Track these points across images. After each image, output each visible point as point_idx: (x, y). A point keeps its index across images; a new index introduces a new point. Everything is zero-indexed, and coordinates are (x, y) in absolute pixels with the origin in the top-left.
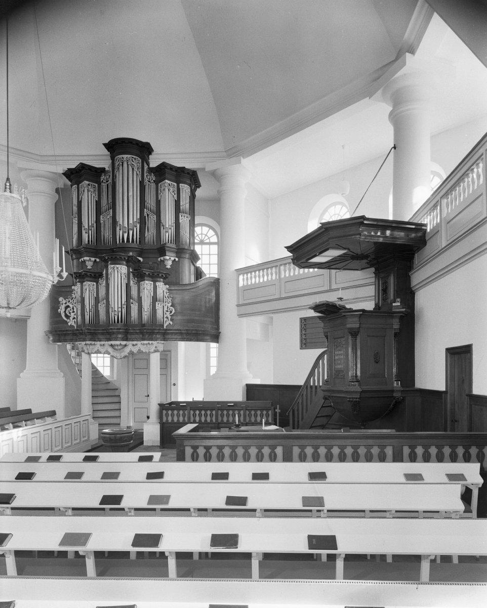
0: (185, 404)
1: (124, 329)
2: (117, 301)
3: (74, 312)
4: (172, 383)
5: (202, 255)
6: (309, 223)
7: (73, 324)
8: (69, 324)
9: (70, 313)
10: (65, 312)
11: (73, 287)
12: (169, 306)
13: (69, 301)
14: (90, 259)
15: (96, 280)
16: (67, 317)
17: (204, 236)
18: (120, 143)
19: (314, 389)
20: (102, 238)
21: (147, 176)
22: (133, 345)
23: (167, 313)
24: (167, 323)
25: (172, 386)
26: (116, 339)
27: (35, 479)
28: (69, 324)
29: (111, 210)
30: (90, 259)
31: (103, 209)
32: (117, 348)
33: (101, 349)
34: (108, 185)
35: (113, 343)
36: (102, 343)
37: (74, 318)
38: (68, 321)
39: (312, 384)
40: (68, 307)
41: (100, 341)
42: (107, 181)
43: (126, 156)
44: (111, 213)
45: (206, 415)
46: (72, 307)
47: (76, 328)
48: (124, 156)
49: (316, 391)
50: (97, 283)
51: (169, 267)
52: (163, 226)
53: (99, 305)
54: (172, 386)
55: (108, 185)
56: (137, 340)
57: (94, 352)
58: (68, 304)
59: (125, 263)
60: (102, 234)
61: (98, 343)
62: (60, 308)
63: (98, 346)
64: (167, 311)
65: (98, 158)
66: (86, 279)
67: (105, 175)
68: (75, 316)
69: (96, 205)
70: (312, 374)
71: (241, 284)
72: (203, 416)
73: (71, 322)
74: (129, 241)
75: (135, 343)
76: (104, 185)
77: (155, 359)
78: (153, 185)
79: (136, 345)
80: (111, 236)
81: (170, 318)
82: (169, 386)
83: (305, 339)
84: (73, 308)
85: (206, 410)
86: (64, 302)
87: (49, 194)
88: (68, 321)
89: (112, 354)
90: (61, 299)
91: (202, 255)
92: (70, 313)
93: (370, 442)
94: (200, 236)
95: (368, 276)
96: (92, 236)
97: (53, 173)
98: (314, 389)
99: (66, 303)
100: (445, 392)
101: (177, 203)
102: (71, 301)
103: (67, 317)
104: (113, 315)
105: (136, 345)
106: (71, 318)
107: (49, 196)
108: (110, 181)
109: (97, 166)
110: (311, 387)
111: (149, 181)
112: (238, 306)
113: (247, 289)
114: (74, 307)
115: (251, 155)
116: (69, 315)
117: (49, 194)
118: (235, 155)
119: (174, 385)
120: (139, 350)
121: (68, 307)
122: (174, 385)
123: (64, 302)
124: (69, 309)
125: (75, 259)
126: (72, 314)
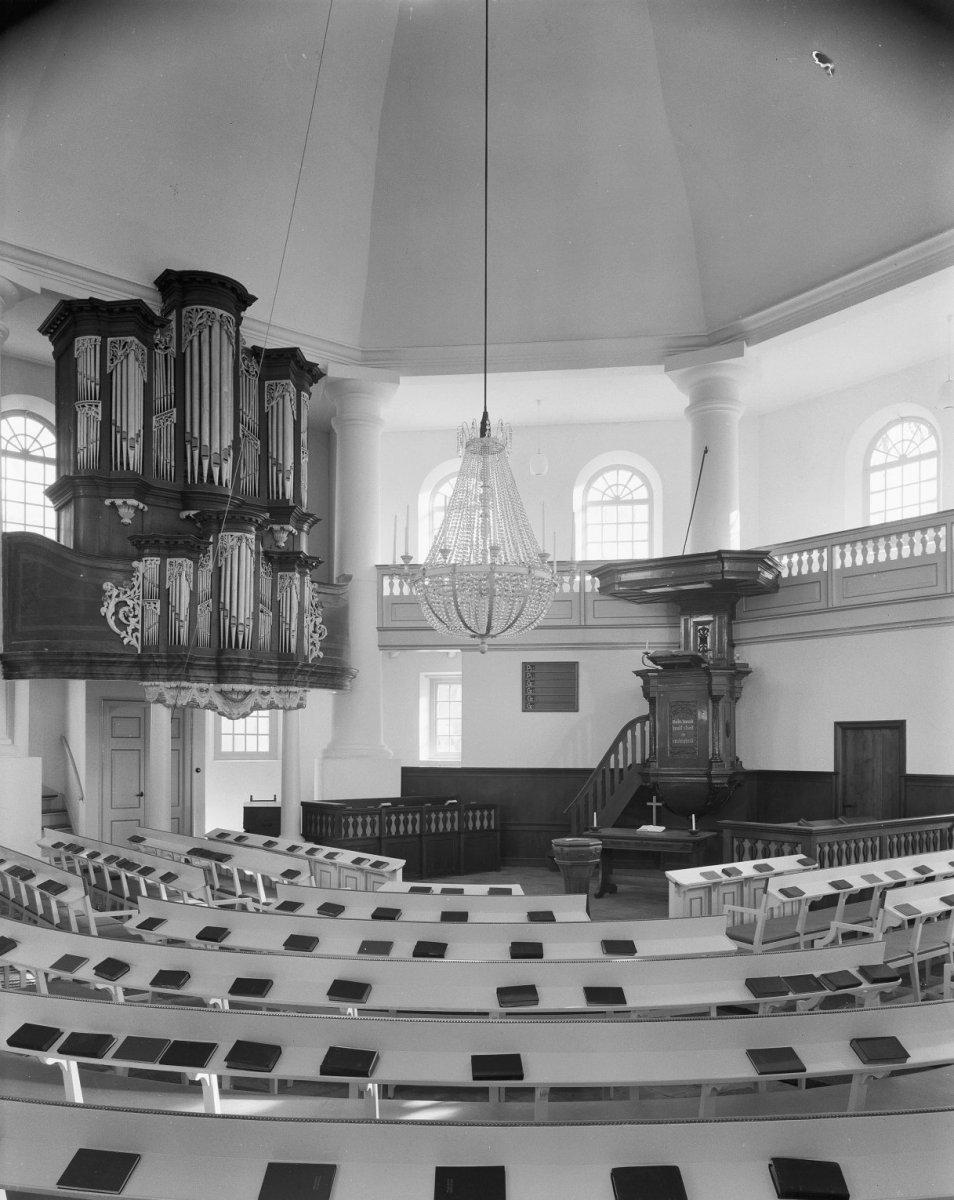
3: (135, 616)
4: (194, 769)
5: (45, 485)
6: (420, 496)
8: (125, 641)
9: (127, 618)
10: (116, 613)
11: (135, 564)
12: (317, 624)
13: (126, 592)
14: (125, 503)
15: (195, 556)
16: (122, 626)
18: (200, 282)
19: (617, 775)
20: (154, 464)
22: (201, 690)
24: (315, 654)
25: (195, 774)
27: (318, 951)
28: (125, 641)
29: (175, 410)
30: (125, 503)
32: (234, 696)
33: (265, 702)
34: (166, 356)
35: (226, 687)
36: (204, 686)
37: (135, 630)
38: (123, 634)
39: (612, 766)
40: (125, 604)
42: (166, 348)
43: (221, 312)
44: (175, 416)
45: (406, 823)
46: (131, 606)
48: (216, 310)
49: (621, 778)
50: (196, 562)
52: (277, 464)
54: (195, 774)
55: (166, 356)
58: (123, 598)
59: (253, 529)
60: (154, 455)
61: (196, 685)
62: (106, 604)
63: (195, 692)
64: (315, 632)
65: (22, 255)
67: (162, 334)
68: (139, 627)
69: (111, 383)
70: (613, 749)
71: (386, 592)
72: (360, 826)
73: (129, 639)
74: (213, 482)
75: (265, 688)
76: (159, 353)
78: (255, 381)
79: (188, 688)
81: (318, 645)
84: (134, 608)
88: (123, 634)
90: (107, 586)
91: (45, 485)
97: (14, 284)
98: (617, 775)
99: (118, 596)
100: (835, 773)
101: (148, 389)
102: (128, 593)
103: (122, 626)
105: (207, 690)
106: (129, 630)
108: (173, 349)
111: (247, 371)
112: (379, 629)
113: (397, 602)
114: (136, 607)
115: (416, 374)
116: (125, 621)
118: (18, 262)
119: (198, 771)
120: (193, 700)
121: (125, 604)
124: (126, 609)
126: (133, 621)
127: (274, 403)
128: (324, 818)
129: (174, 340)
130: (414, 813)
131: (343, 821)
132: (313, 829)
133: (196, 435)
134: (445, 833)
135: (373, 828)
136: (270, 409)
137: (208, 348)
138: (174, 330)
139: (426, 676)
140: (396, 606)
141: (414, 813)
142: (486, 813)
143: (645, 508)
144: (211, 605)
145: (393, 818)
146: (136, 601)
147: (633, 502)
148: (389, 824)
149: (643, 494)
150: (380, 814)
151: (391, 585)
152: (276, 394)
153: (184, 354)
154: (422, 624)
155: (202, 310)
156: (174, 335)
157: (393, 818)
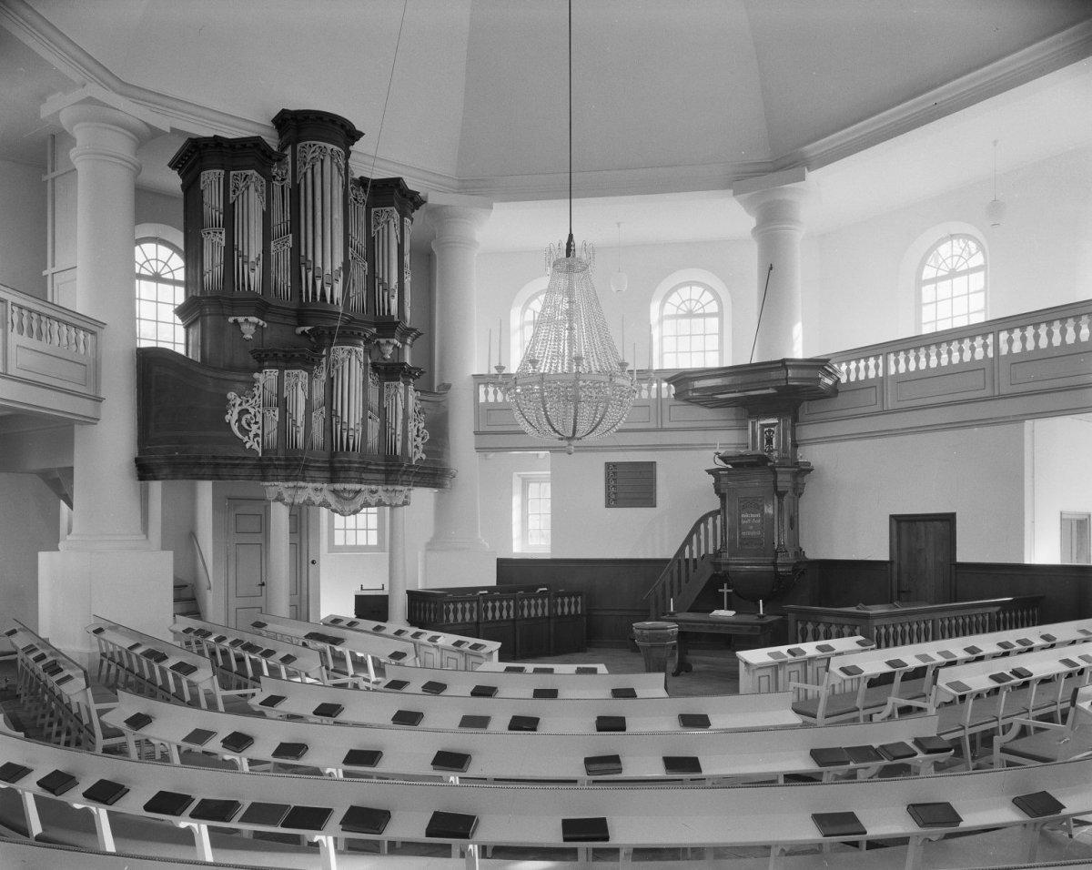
0: (486, 592)
1: (386, 465)
2: (353, 411)
3: (256, 423)
4: (310, 560)
6: (512, 311)
7: (255, 446)
8: (248, 446)
9: (249, 425)
10: (239, 420)
11: (256, 375)
13: (248, 401)
14: (246, 320)
17: (161, 265)
19: (691, 564)
21: (352, 189)
22: (316, 490)
23: (418, 439)
24: (418, 456)
26: (347, 480)
27: (423, 724)
28: (248, 446)
29: (291, 235)
30: (246, 320)
31: (275, 230)
32: (346, 495)
33: (374, 500)
35: (338, 486)
36: (318, 485)
37: (256, 435)
38: (246, 439)
40: (247, 411)
41: (314, 481)
42: (283, 180)
43: (331, 146)
46: (253, 413)
47: (260, 455)
51: (248, 336)
53: (313, 414)
56: (378, 484)
57: (401, 503)
58: (245, 406)
62: (230, 412)
63: (310, 491)
66: (266, 364)
67: (279, 168)
68: (260, 432)
70: (688, 541)
71: (482, 399)
73: (252, 444)
74: (326, 300)
76: (277, 185)
77: (280, 516)
78: (363, 209)
80: (289, 284)
81: (421, 447)
82: (305, 567)
83: (615, 494)
84: (255, 415)
85: (570, 597)
86: (238, 401)
87: (135, 166)
88: (246, 439)
89: (333, 507)
90: (231, 395)
92: (249, 425)
93: (842, 620)
94: (146, 265)
95: (722, 418)
96: (383, 300)
97: (146, 124)
98: (691, 564)
99: (240, 405)
100: (891, 562)
104: (345, 434)
106: (251, 435)
107: (129, 165)
108: (289, 180)
109: (230, 137)
110: (687, 560)
111: (356, 200)
112: (476, 433)
113: (491, 409)
114: (257, 414)
116: (247, 427)
117: (135, 166)
119: (313, 562)
121: (247, 411)
122: (313, 562)
123: (238, 401)
124: (248, 416)
125: (210, 315)
126: (254, 427)
127: (380, 228)
129: (290, 172)
139: (519, 476)
143: (715, 321)
145: (490, 604)
147: (704, 315)
148: (486, 610)
149: (713, 308)
150: (478, 601)
151: (487, 393)
154: (512, 429)
155: (314, 145)
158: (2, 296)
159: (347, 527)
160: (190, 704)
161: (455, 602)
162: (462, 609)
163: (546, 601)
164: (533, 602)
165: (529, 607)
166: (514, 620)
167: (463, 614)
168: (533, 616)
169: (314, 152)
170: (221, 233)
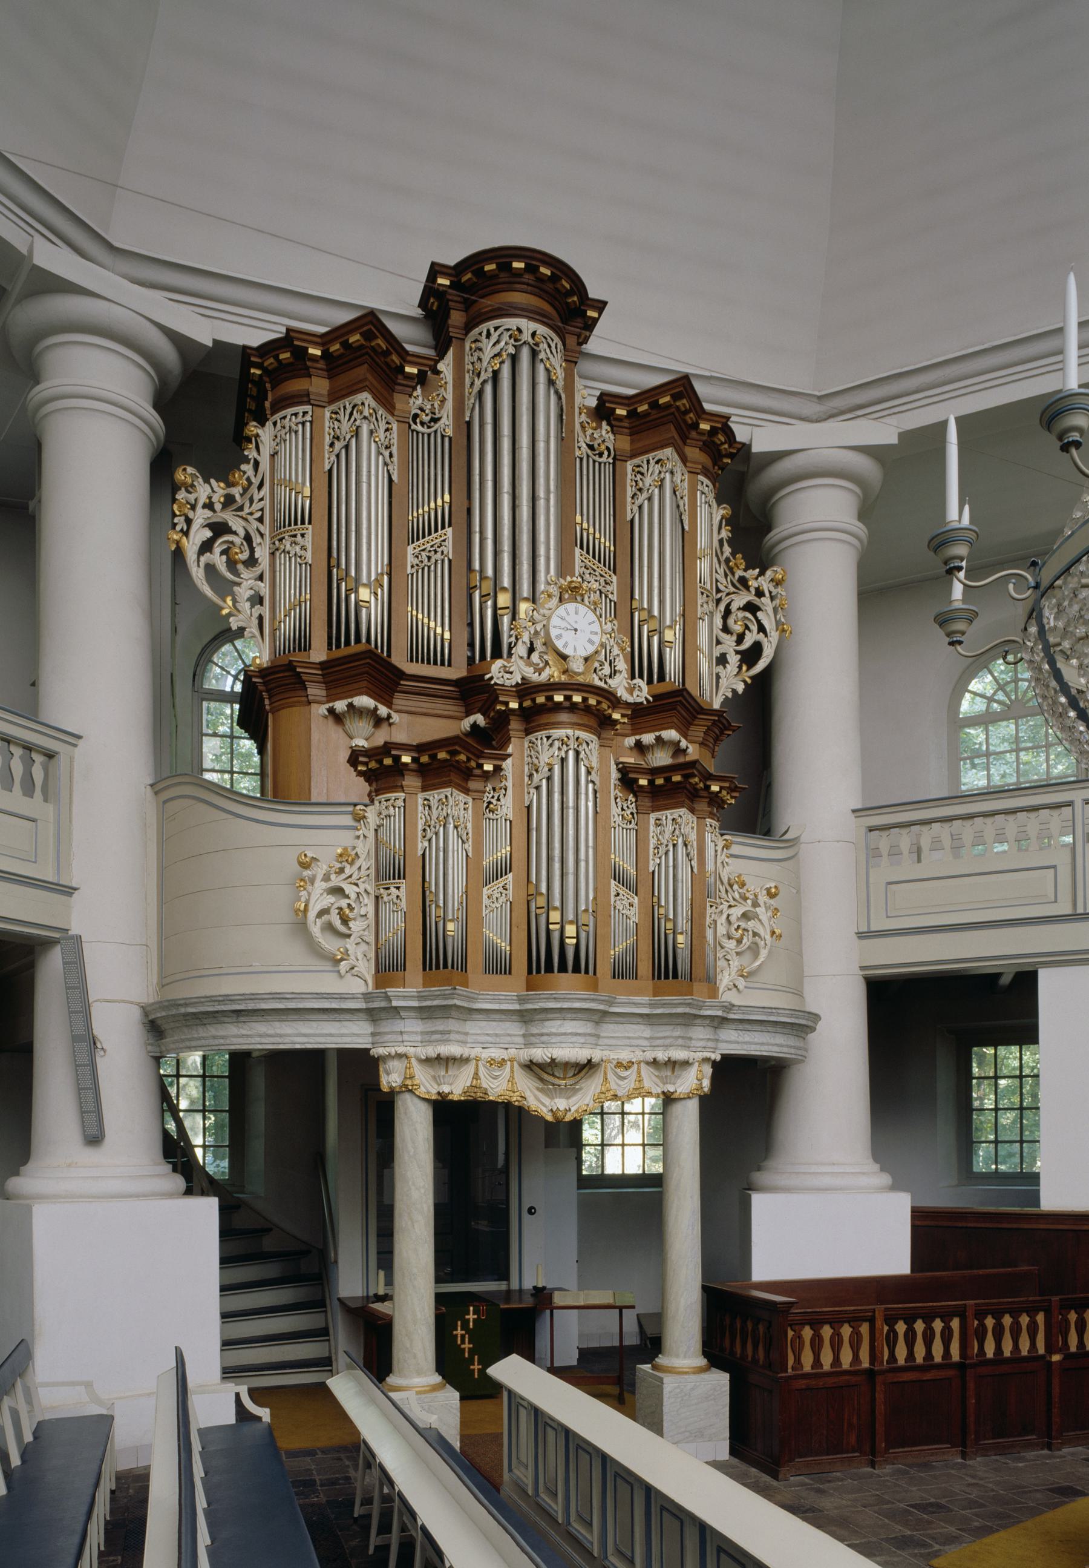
42: (435, 420)
44: (449, 543)
67: (425, 396)
84: (248, 538)
127: (642, 498)
128: (750, 1326)
129: (449, 405)
130: (946, 1318)
131: (790, 1333)
132: (738, 1349)
133: (490, 572)
134: (1016, 1359)
135: (855, 1348)
136: (636, 509)
137: (517, 1188)
138: (450, 387)
140: (893, 887)
141: (946, 1318)
142: (1025, 1320)
144: (510, 887)
145: (990, 1322)
146: (255, 524)
148: (892, 1340)
150: (872, 1321)
152: (648, 480)
153: (469, 424)
155: (496, 329)
156: (449, 396)
157: (990, 1322)
158: (4, 730)
159: (641, 1148)
160: (976, 617)
161: (816, 1323)
162: (906, 1334)
163: (1040, 1318)
164: (938, 1325)
165: (817, 1344)
166: (961, 1366)
167: (928, 1343)
168: (1025, 1352)
169: (498, 342)
170: (398, 888)
